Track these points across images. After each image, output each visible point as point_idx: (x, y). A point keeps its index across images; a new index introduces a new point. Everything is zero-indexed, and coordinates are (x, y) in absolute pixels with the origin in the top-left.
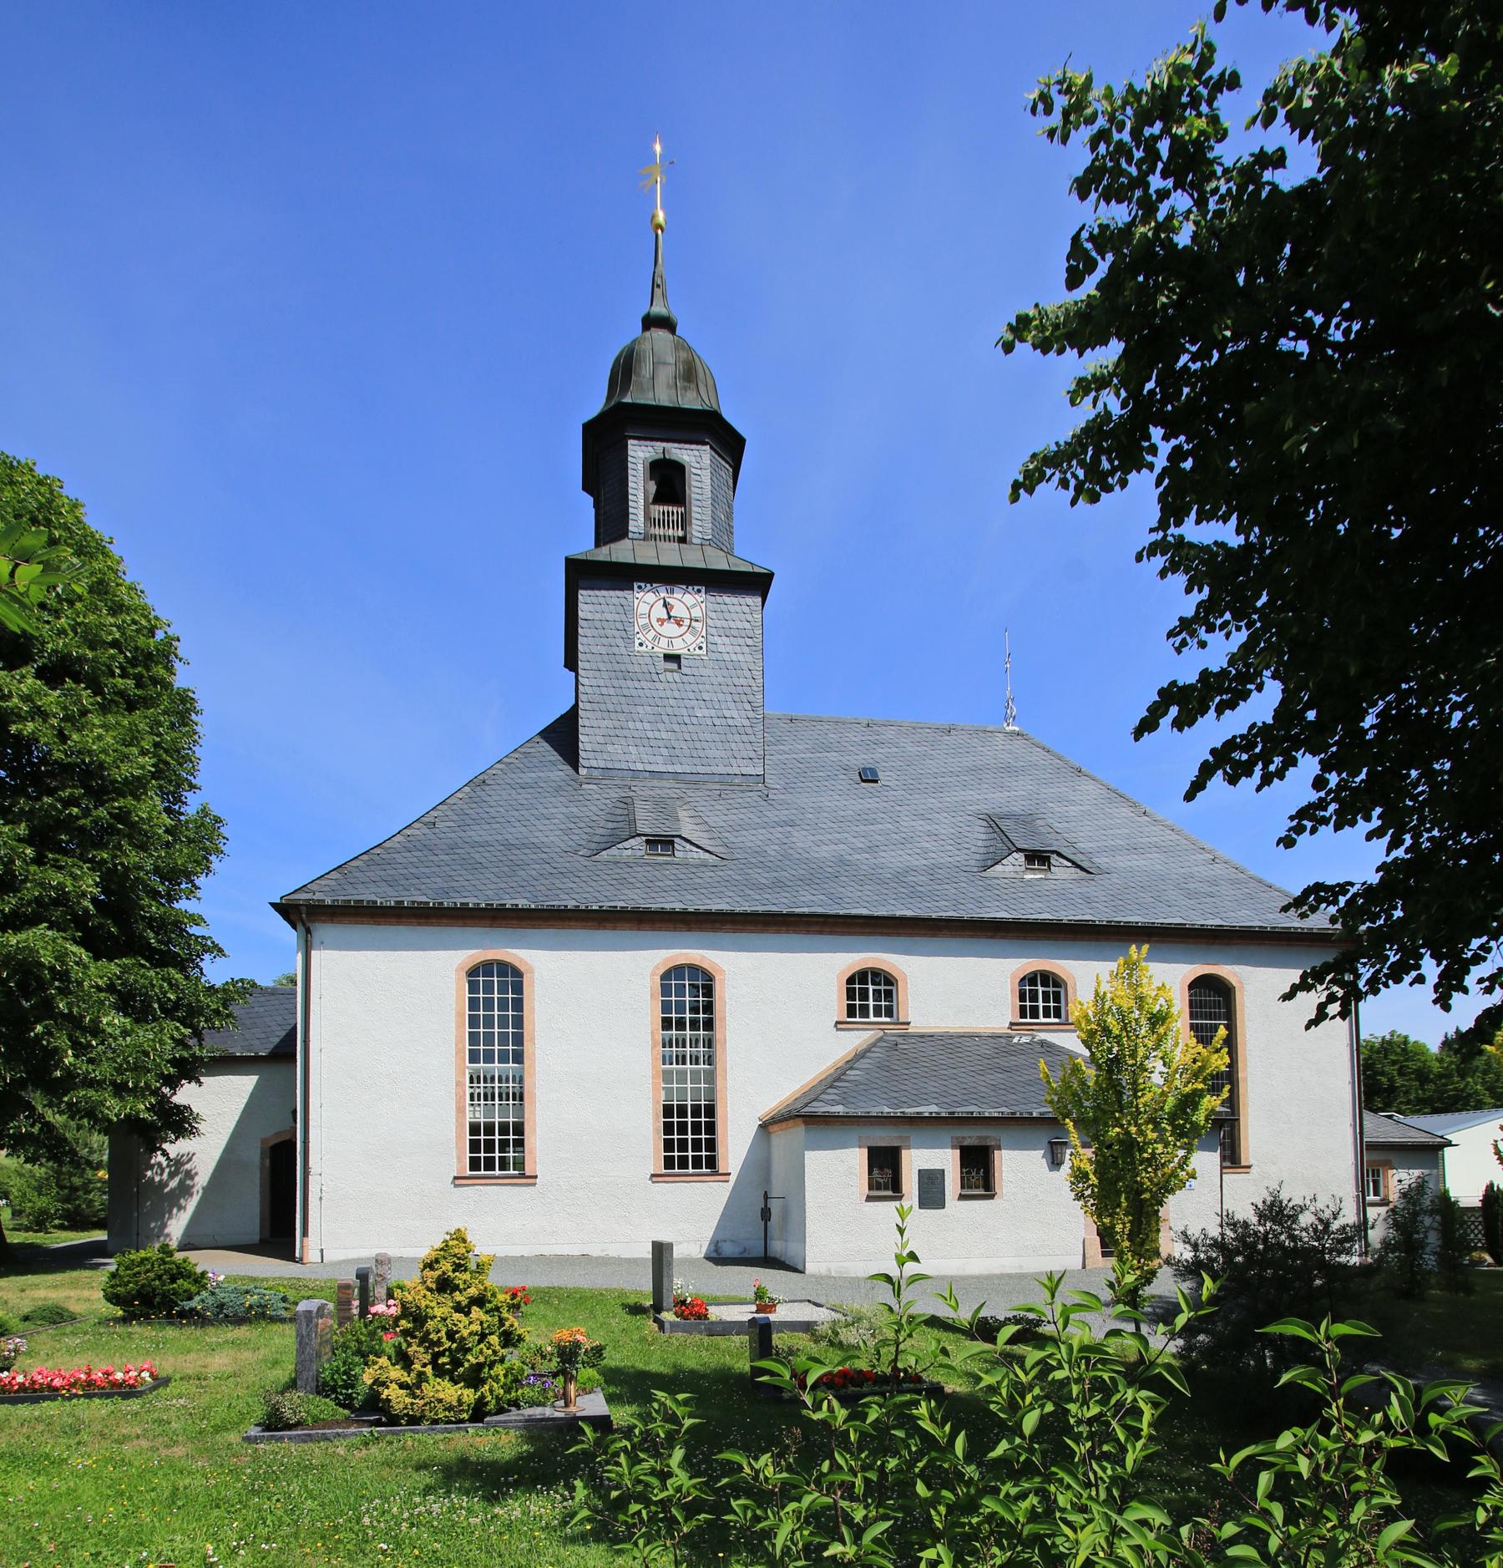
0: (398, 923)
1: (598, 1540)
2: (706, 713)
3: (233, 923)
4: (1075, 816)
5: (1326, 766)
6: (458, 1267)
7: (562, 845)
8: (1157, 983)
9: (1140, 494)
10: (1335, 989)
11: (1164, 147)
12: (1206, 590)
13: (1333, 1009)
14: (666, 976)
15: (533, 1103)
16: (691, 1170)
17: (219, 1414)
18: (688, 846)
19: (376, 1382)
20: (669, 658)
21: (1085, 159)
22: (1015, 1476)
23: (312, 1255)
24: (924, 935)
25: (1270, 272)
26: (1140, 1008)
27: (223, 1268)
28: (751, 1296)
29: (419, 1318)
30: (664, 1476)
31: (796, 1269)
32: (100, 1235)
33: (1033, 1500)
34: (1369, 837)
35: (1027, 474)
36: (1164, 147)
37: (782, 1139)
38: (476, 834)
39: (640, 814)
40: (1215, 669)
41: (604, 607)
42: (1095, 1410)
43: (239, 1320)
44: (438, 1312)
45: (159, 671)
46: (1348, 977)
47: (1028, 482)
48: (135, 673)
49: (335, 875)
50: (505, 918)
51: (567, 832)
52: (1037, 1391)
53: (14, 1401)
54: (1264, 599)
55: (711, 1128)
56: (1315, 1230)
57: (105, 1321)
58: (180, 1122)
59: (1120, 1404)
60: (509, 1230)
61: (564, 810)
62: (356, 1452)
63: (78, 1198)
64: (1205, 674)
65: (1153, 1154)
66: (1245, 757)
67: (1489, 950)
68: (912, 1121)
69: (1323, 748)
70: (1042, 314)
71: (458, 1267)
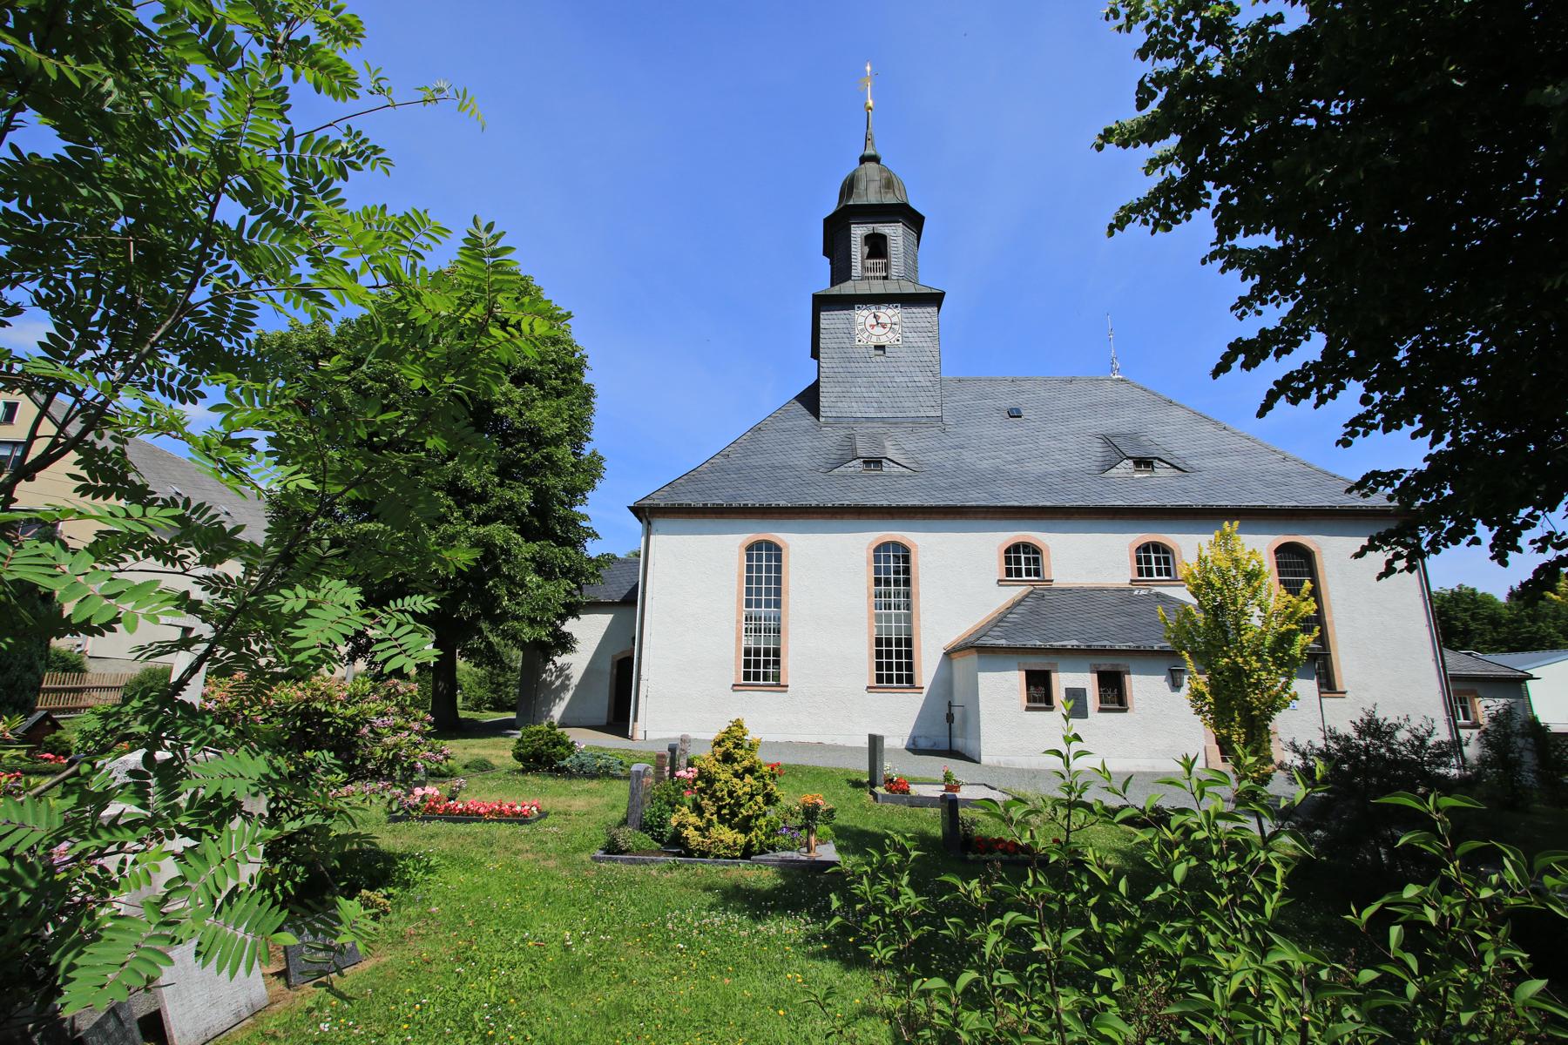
1: (832, 958)
3: (605, 519)
4: (1167, 432)
5: (1370, 388)
6: (737, 746)
9: (1201, 226)
10: (1400, 549)
11: (1196, 24)
12: (1257, 278)
13: (1400, 564)
14: (877, 550)
17: (578, 839)
19: (680, 824)
20: (876, 347)
21: (1144, 38)
22: (1172, 917)
23: (639, 735)
25: (1281, 81)
26: (1237, 568)
27: (585, 740)
28: (941, 778)
29: (710, 780)
30: (896, 895)
31: (971, 758)
32: (512, 715)
33: (1186, 938)
34: (1414, 436)
35: (1118, 219)
36: (1196, 24)
37: (962, 664)
38: (755, 460)
39: (859, 444)
40: (1271, 328)
42: (1233, 867)
43: (592, 776)
44: (723, 777)
46: (1410, 541)
47: (1120, 223)
48: (562, 376)
52: (1182, 848)
53: (455, 821)
54: (1303, 279)
55: (909, 655)
56: (1413, 745)
57: (512, 772)
58: (564, 643)
59: (1254, 863)
60: (771, 722)
62: (664, 874)
64: (1263, 332)
65: (1259, 680)
66: (1302, 385)
67: (1538, 518)
68: (1040, 649)
69: (1367, 375)
70: (1121, 126)
71: (737, 746)
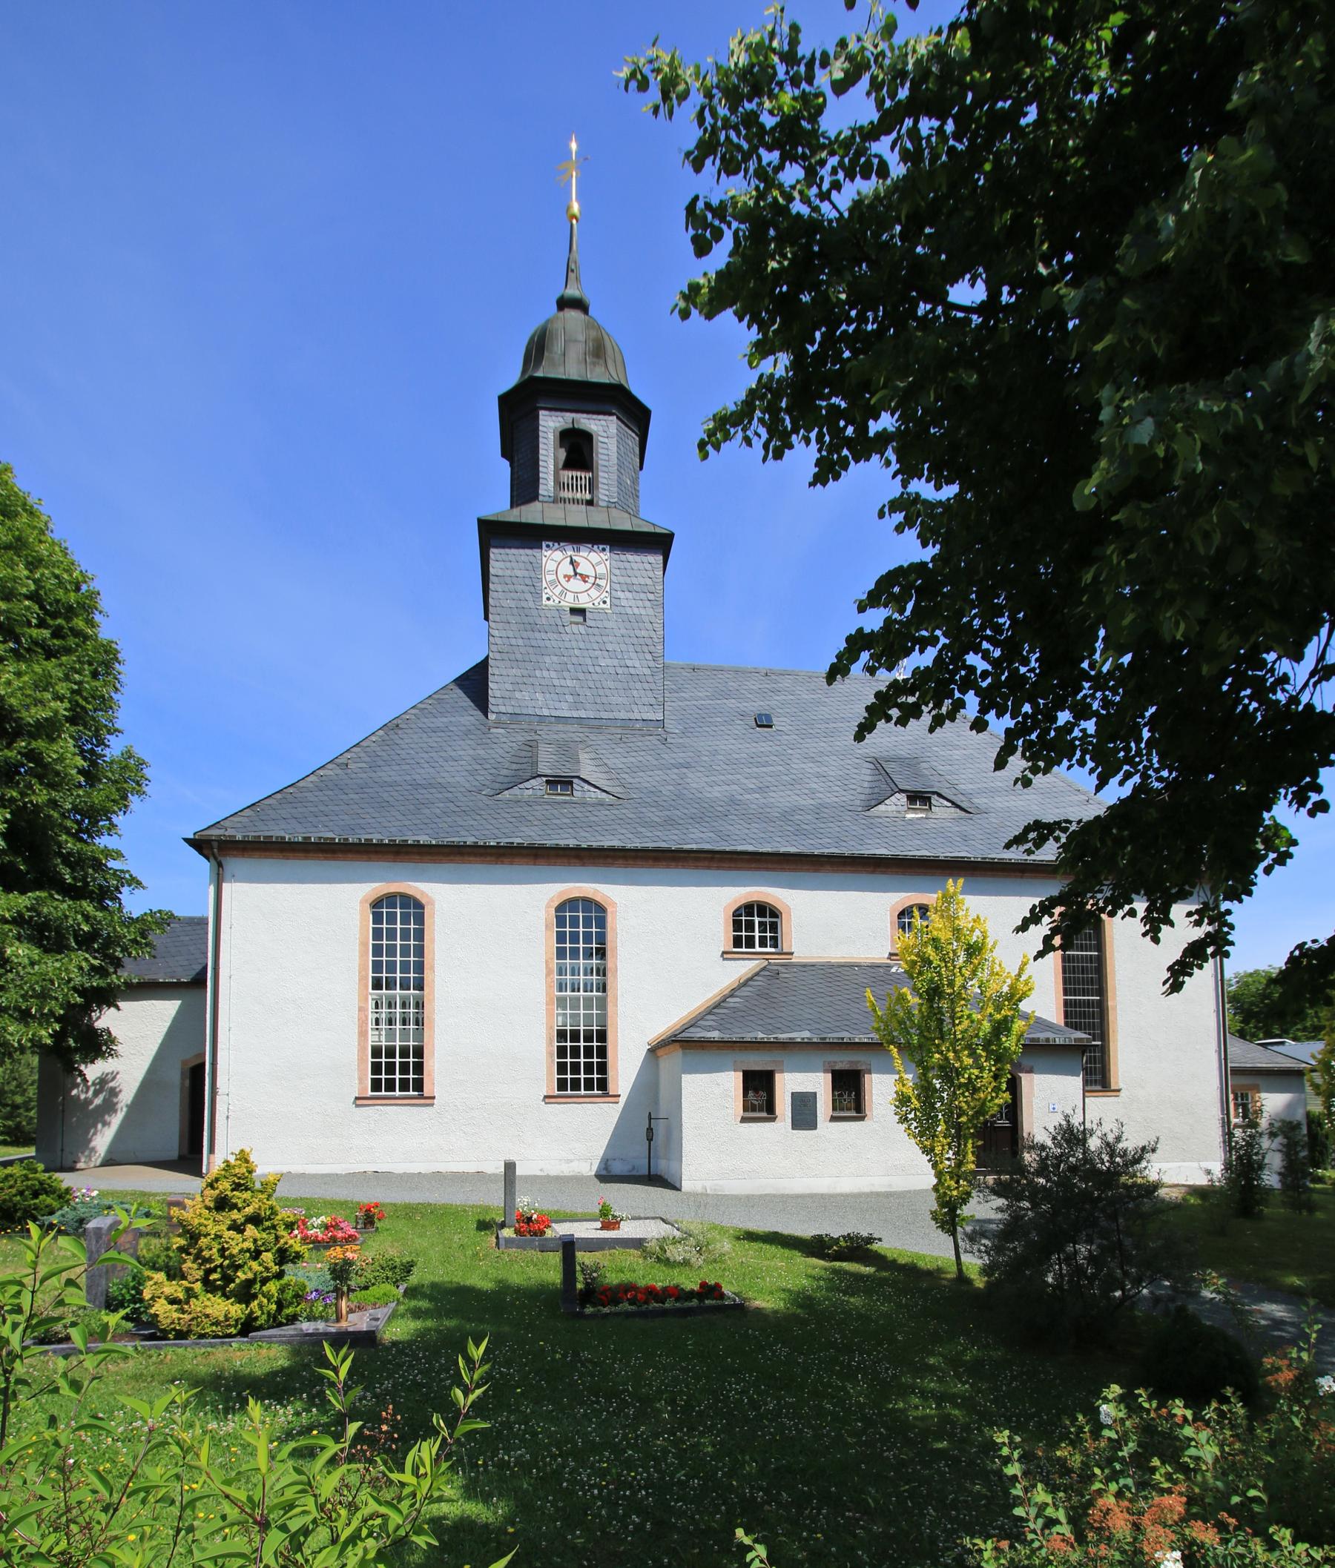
0: (306, 858)
2: (609, 662)
3: (150, 860)
7: (467, 785)
8: (973, 915)
12: (938, 546)
14: (560, 908)
15: (432, 1028)
16: (583, 1092)
18: (586, 787)
20: (575, 611)
24: (808, 870)
37: (671, 1060)
38: (386, 774)
41: (514, 564)
44: (212, 1229)
45: (79, 623)
48: (57, 623)
49: (248, 812)
50: (407, 853)
51: (472, 773)
55: (602, 1052)
58: (97, 1045)
61: (471, 752)
63: (19, 1115)
68: (750, 1046)
71: (237, 1187)
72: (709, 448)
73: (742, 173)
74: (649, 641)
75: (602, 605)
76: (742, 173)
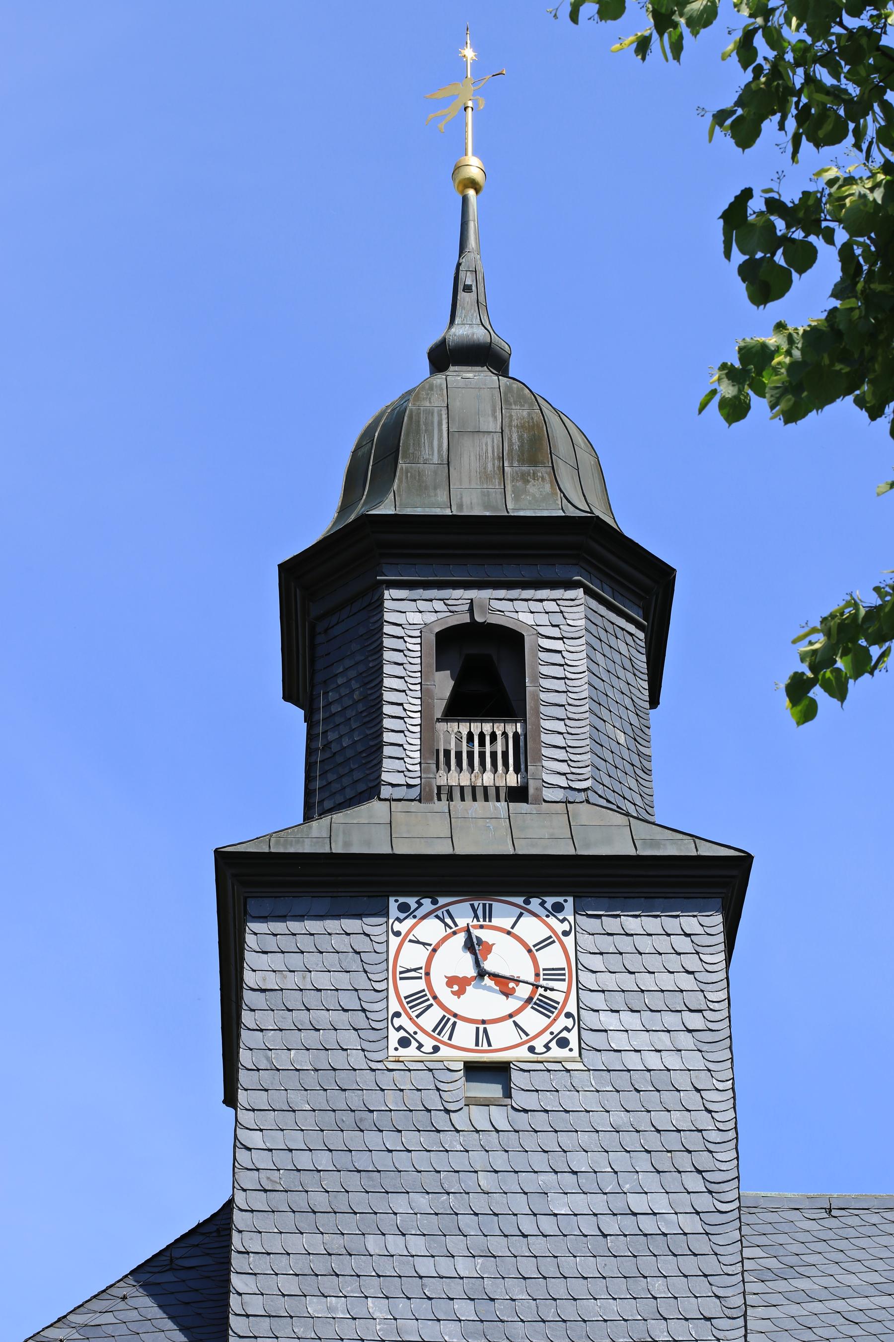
2: (580, 1203)
20: (475, 1071)
41: (312, 960)
72: (817, 693)
73: (850, 139)
74: (693, 1141)
75: (556, 1052)
76: (850, 139)
